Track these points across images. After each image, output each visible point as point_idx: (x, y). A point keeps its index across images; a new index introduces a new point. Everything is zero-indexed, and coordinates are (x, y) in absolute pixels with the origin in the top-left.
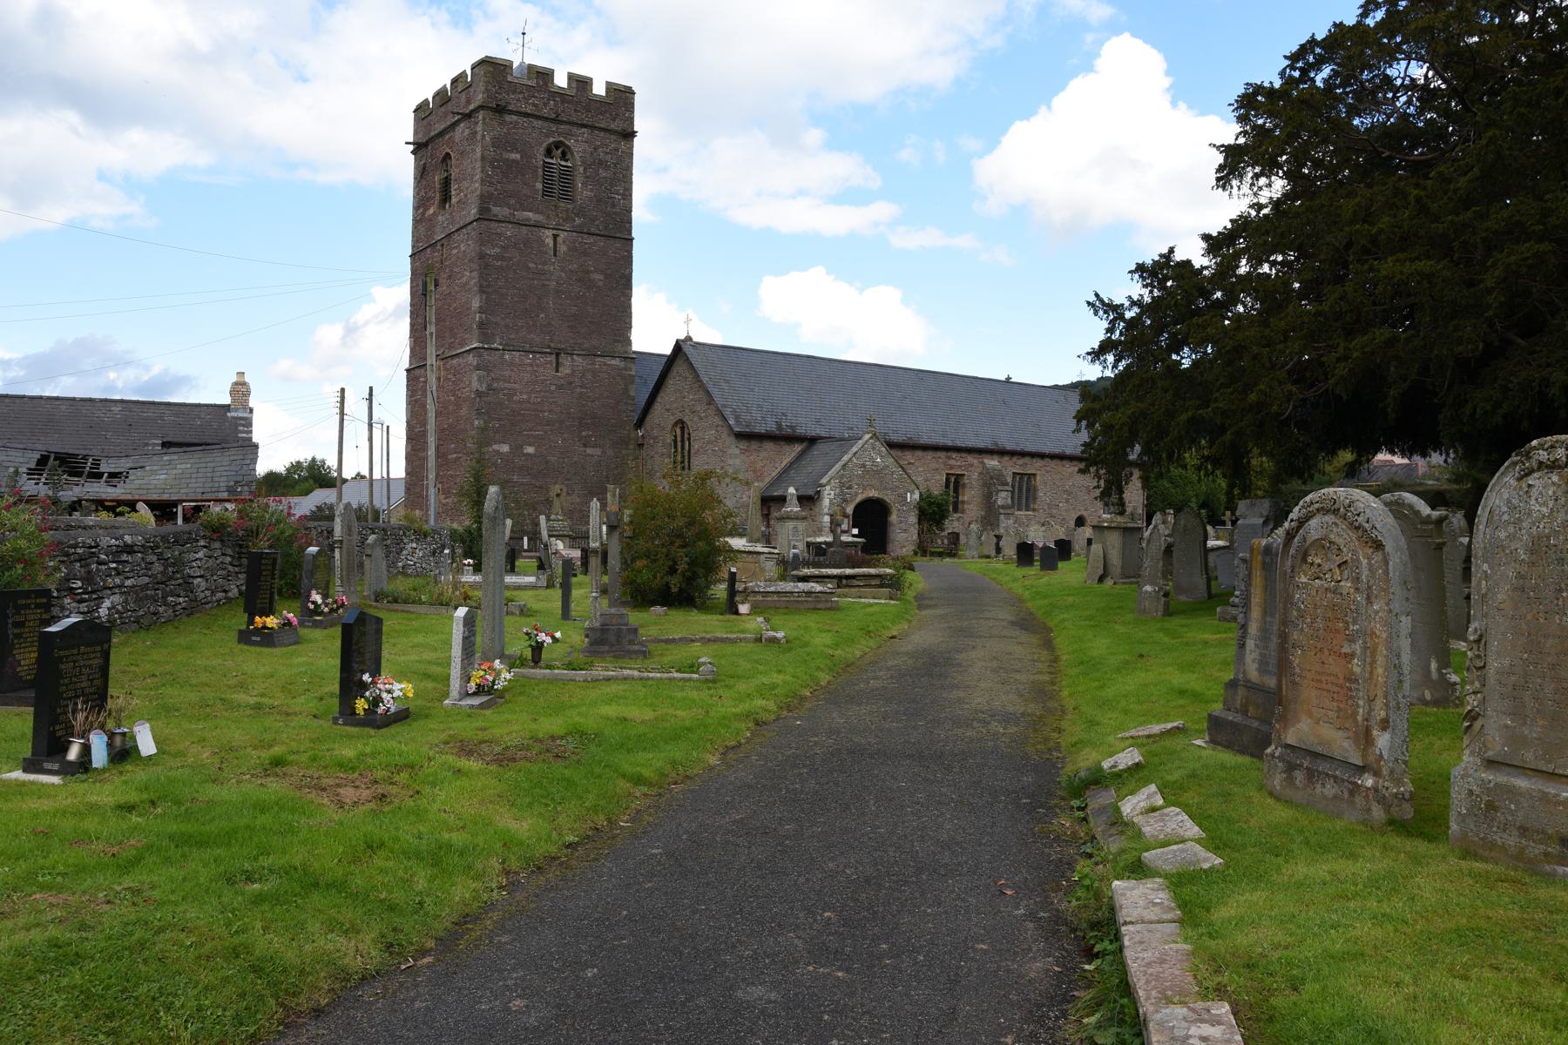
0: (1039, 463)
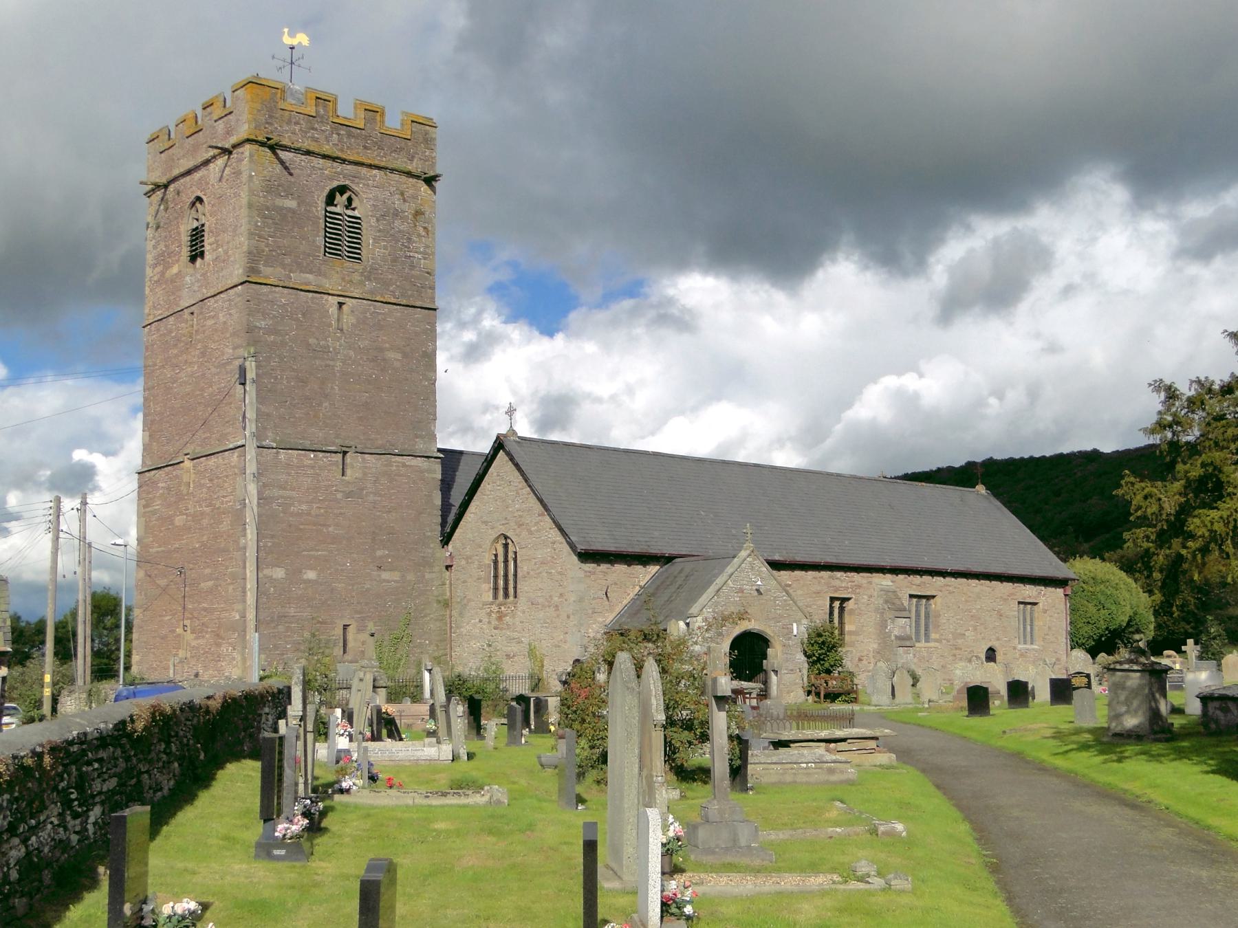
0: (939, 580)
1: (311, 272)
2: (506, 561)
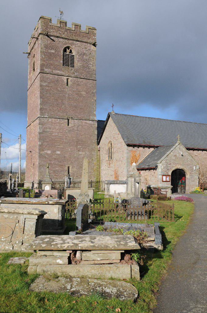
1: (59, 70)
2: (111, 149)
